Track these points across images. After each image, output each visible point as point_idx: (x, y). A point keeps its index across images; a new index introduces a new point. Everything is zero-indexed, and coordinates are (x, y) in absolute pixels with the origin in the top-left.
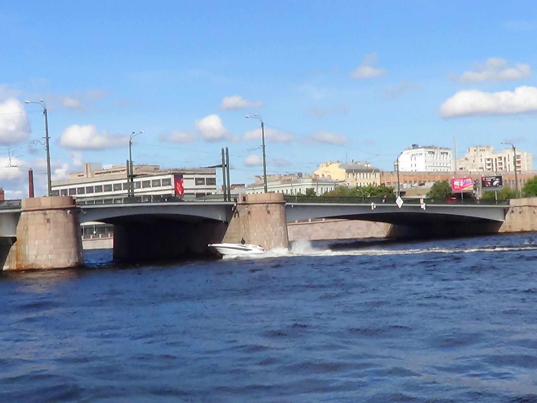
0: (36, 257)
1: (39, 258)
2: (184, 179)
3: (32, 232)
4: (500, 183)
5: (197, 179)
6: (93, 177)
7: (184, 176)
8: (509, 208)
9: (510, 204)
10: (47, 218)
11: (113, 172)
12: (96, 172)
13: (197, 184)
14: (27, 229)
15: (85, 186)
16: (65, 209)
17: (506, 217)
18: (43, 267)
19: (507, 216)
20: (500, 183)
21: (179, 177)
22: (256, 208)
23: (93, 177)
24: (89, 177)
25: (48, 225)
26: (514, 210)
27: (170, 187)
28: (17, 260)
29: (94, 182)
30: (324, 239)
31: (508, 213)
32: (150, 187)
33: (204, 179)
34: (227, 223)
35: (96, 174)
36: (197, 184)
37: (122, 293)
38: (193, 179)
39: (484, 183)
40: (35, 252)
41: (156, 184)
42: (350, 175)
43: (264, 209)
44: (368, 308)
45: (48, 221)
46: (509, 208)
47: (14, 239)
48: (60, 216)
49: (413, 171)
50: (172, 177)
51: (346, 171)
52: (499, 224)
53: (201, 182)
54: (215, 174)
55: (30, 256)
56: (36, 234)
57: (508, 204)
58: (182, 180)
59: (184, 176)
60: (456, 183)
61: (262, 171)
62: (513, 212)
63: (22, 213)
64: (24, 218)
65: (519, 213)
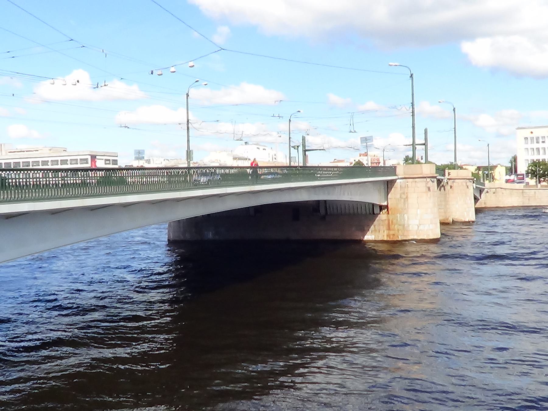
0: (418, 227)
1: (421, 227)
2: (98, 159)
3: (413, 199)
5: (106, 160)
8: (484, 189)
9: (485, 186)
10: (428, 186)
11: (27, 151)
12: (10, 151)
13: (106, 164)
14: (407, 197)
17: (481, 196)
19: (482, 195)
21: (93, 157)
22: (458, 183)
23: (6, 155)
24: (3, 154)
25: (429, 193)
26: (489, 191)
28: (389, 229)
29: (21, 158)
31: (483, 192)
32: (68, 164)
35: (10, 152)
36: (106, 164)
37: (131, 258)
38: (103, 159)
40: (417, 222)
41: (73, 162)
43: (465, 184)
46: (484, 189)
49: (270, 161)
50: (89, 157)
51: (233, 159)
53: (108, 162)
54: (117, 156)
55: (410, 226)
56: (418, 202)
58: (96, 160)
59: (97, 157)
61: (411, 151)
62: (487, 192)
63: (398, 181)
64: (401, 186)
65: (492, 193)
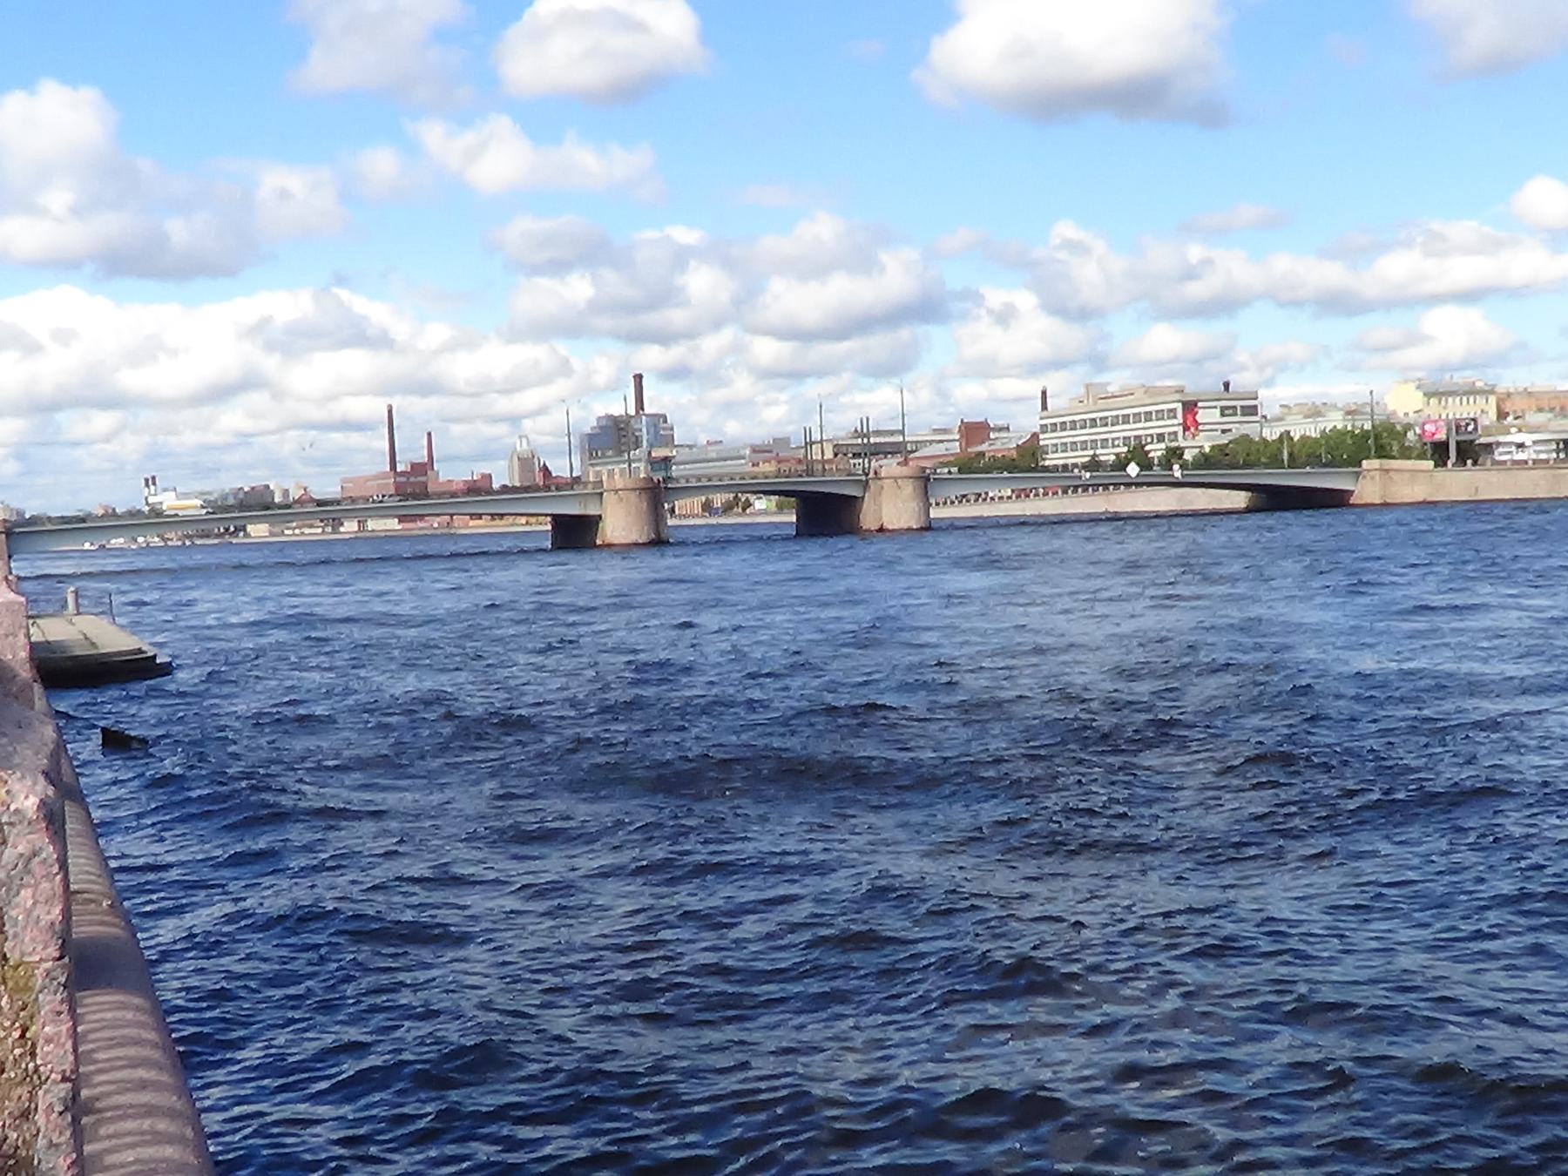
4: (1476, 429)
5: (1223, 409)
6: (1095, 403)
7: (1200, 404)
15: (1143, 410)
16: (635, 489)
18: (616, 542)
20: (1476, 429)
27: (1175, 422)
30: (1429, 499)
33: (1235, 407)
34: (863, 498)
36: (1223, 415)
39: (1458, 427)
41: (1160, 416)
42: (1433, 401)
44: (174, 560)
45: (621, 500)
47: (600, 516)
48: (633, 496)
50: (1179, 406)
52: (1351, 493)
57: (1360, 466)
59: (1200, 404)
60: (1427, 427)
